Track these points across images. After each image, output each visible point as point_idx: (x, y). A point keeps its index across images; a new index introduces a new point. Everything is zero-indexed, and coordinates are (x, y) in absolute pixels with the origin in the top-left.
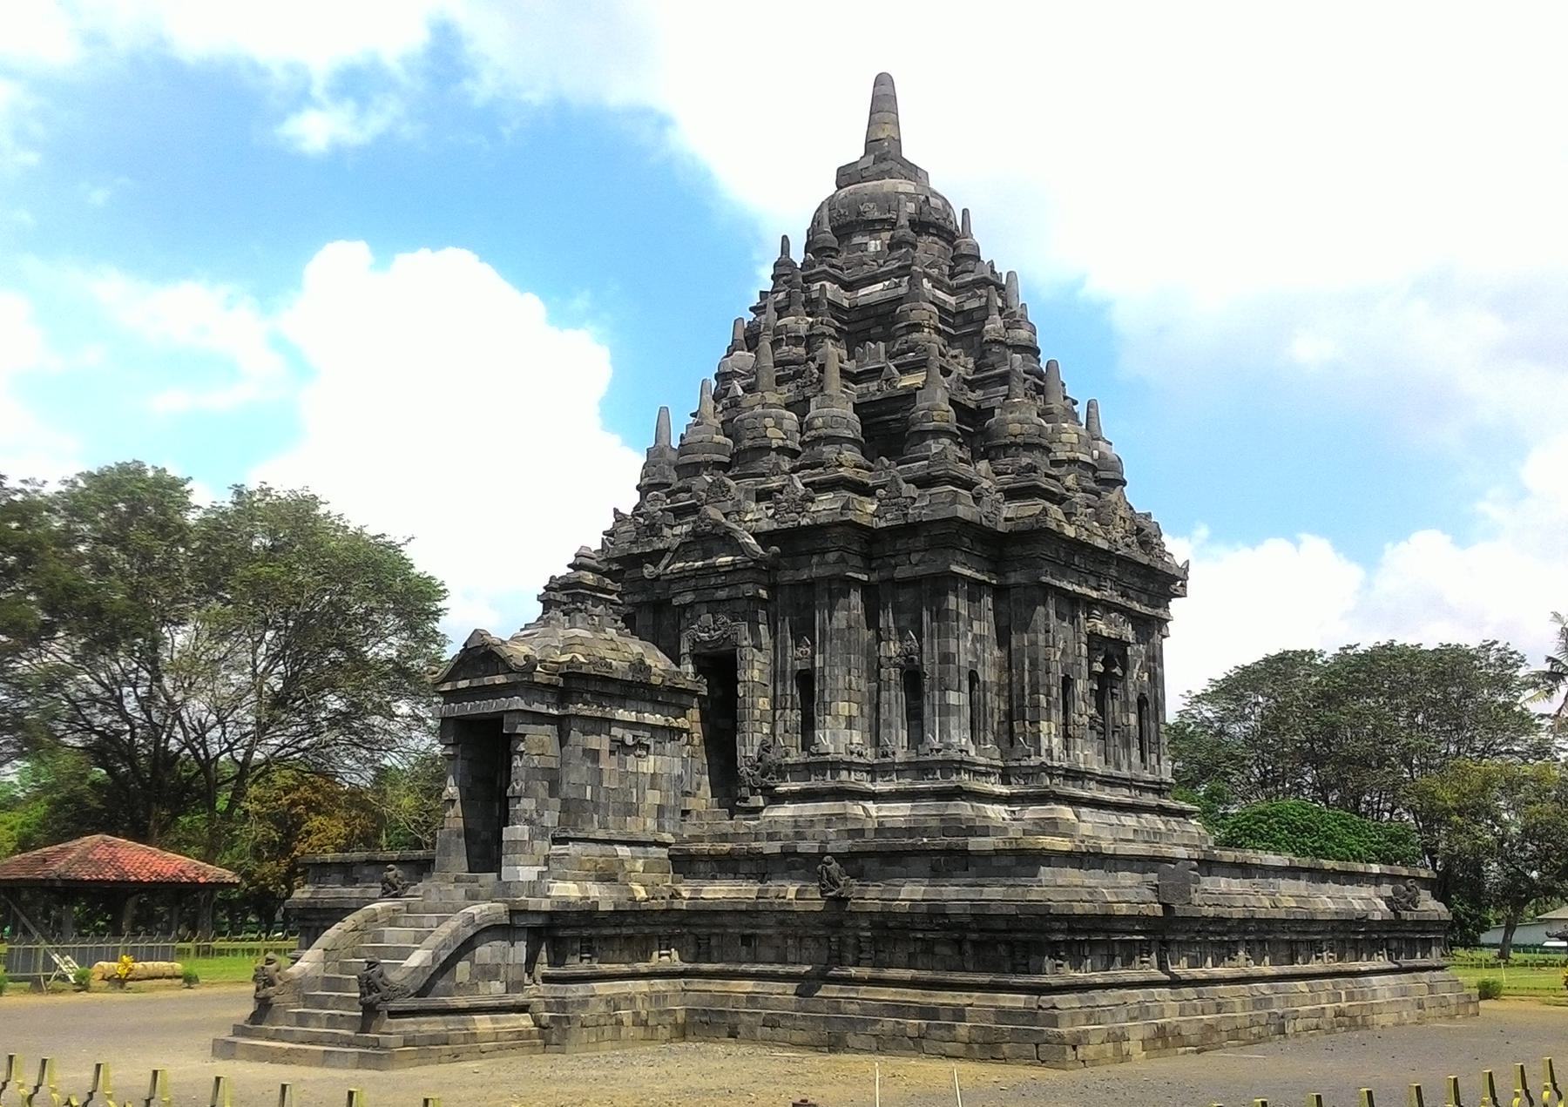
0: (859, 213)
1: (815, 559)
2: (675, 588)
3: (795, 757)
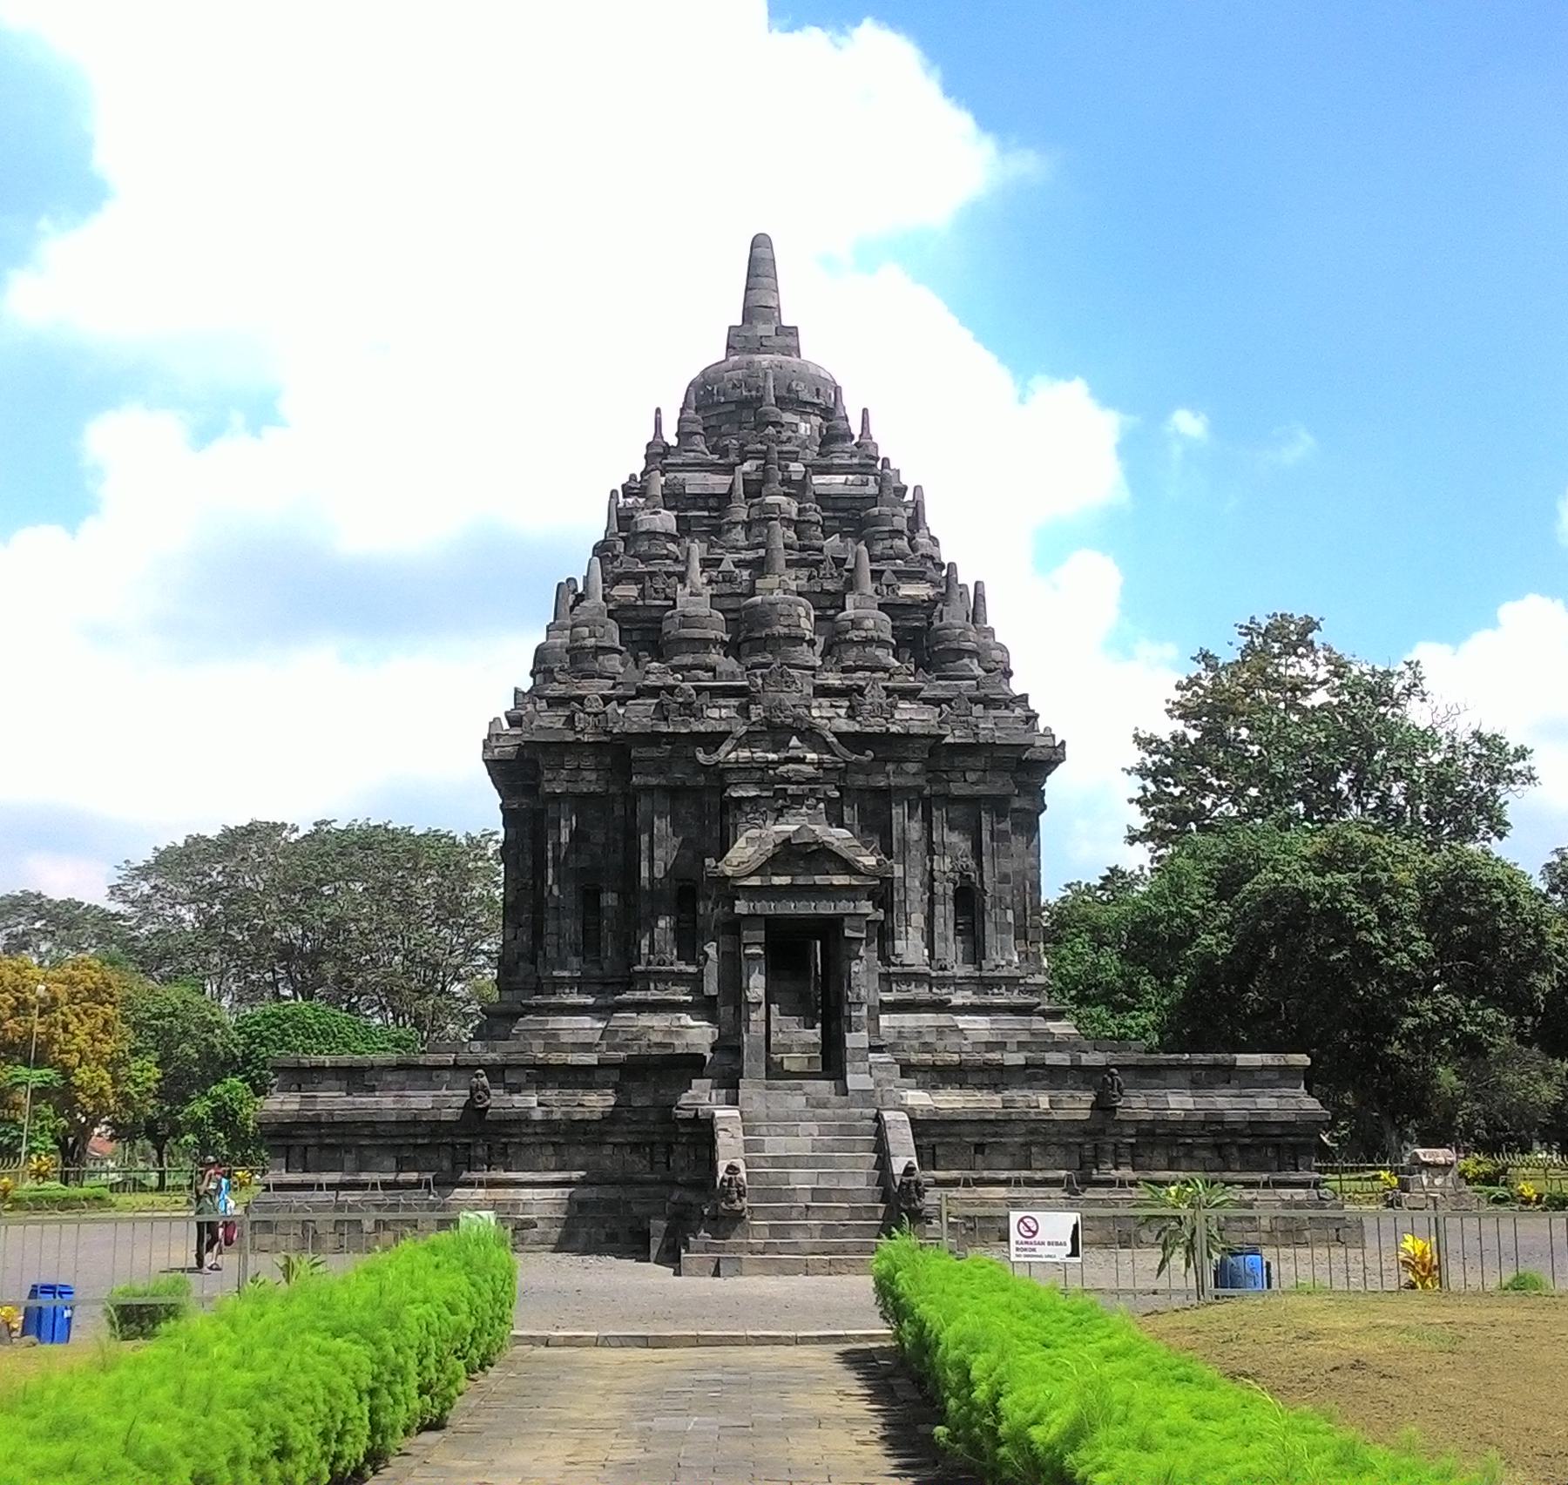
0: (789, 390)
1: (890, 767)
2: (732, 778)
3: (961, 970)
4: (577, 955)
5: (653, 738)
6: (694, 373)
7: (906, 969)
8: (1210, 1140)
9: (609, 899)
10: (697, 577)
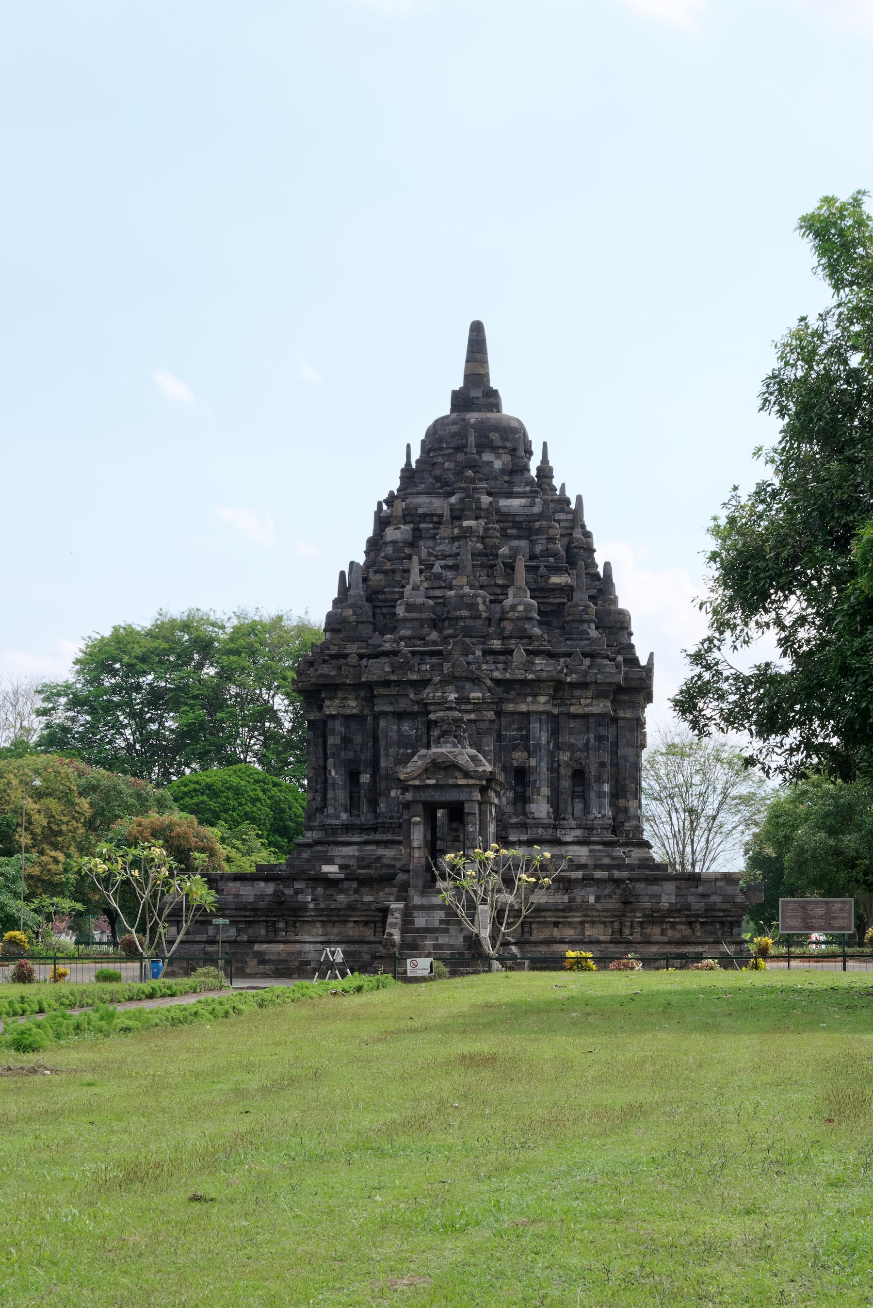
1: (530, 699)
4: (346, 811)
5: (387, 683)
6: (430, 422)
8: (684, 919)
9: (365, 778)
10: (415, 577)
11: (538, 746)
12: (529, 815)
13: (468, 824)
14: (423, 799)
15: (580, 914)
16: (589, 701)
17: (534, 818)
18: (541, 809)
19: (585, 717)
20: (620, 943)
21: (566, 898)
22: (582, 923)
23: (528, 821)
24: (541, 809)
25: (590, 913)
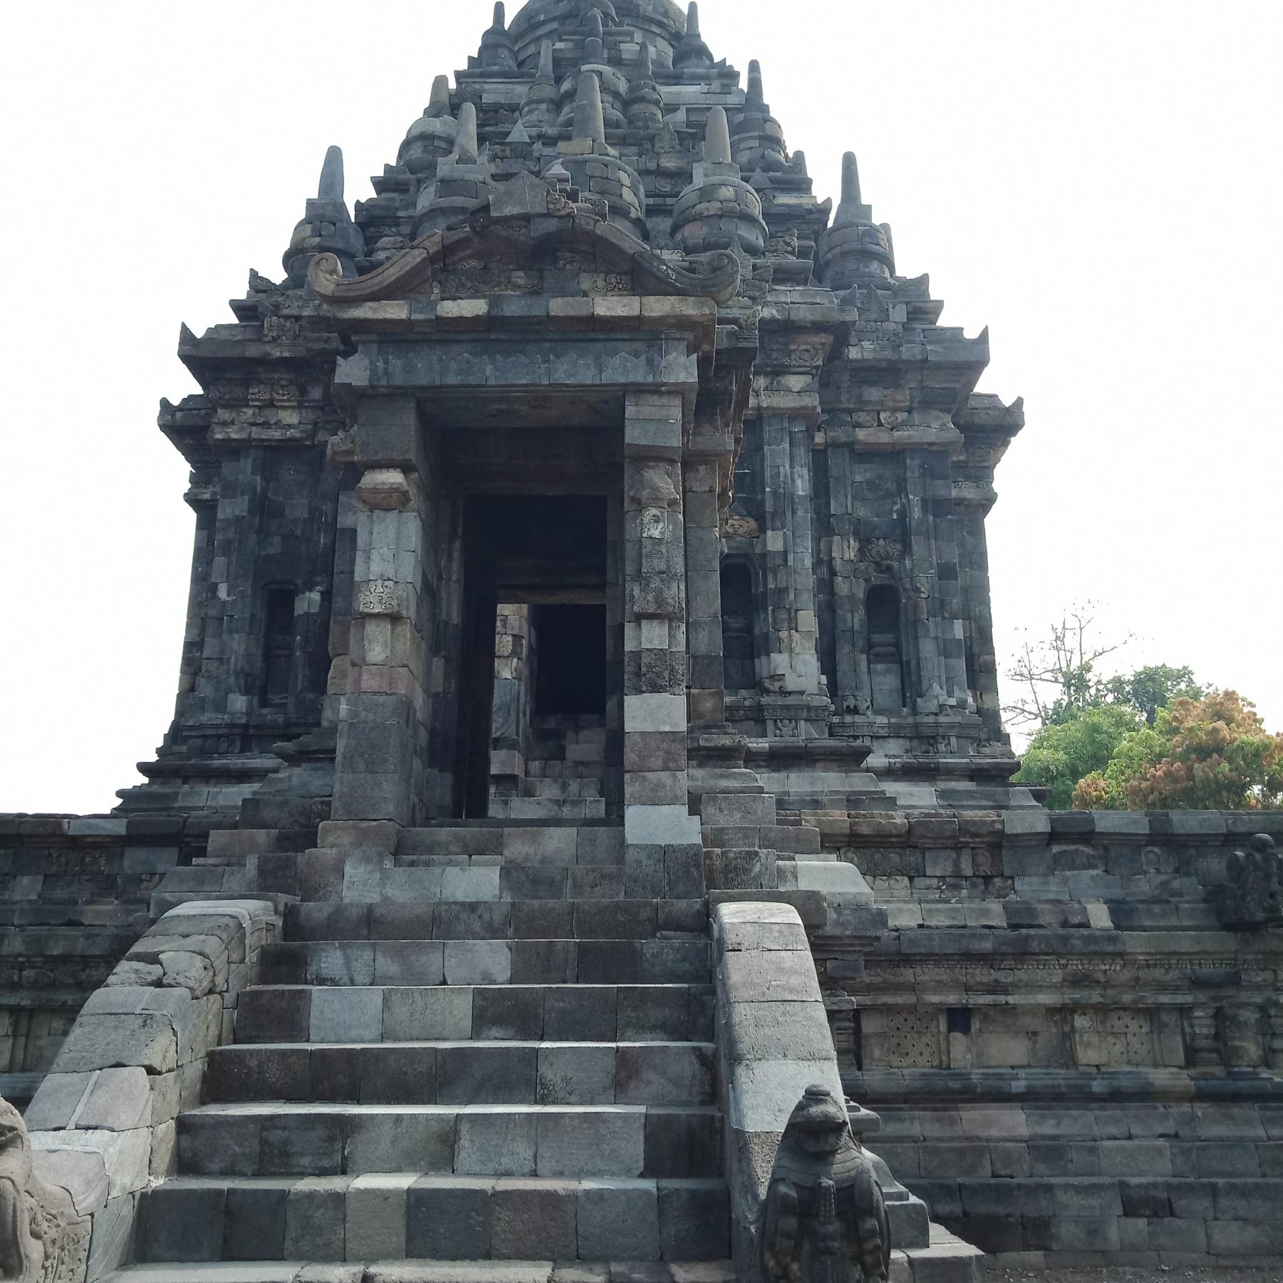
4: (247, 692)
7: (791, 700)
11: (786, 499)
12: (767, 683)
13: (640, 507)
14: (423, 380)
15: (1058, 976)
16: (901, 416)
17: (784, 693)
18: (797, 666)
19: (895, 455)
20: (1237, 1098)
21: (995, 913)
22: (1063, 1012)
23: (765, 700)
24: (797, 666)
25: (1100, 969)
